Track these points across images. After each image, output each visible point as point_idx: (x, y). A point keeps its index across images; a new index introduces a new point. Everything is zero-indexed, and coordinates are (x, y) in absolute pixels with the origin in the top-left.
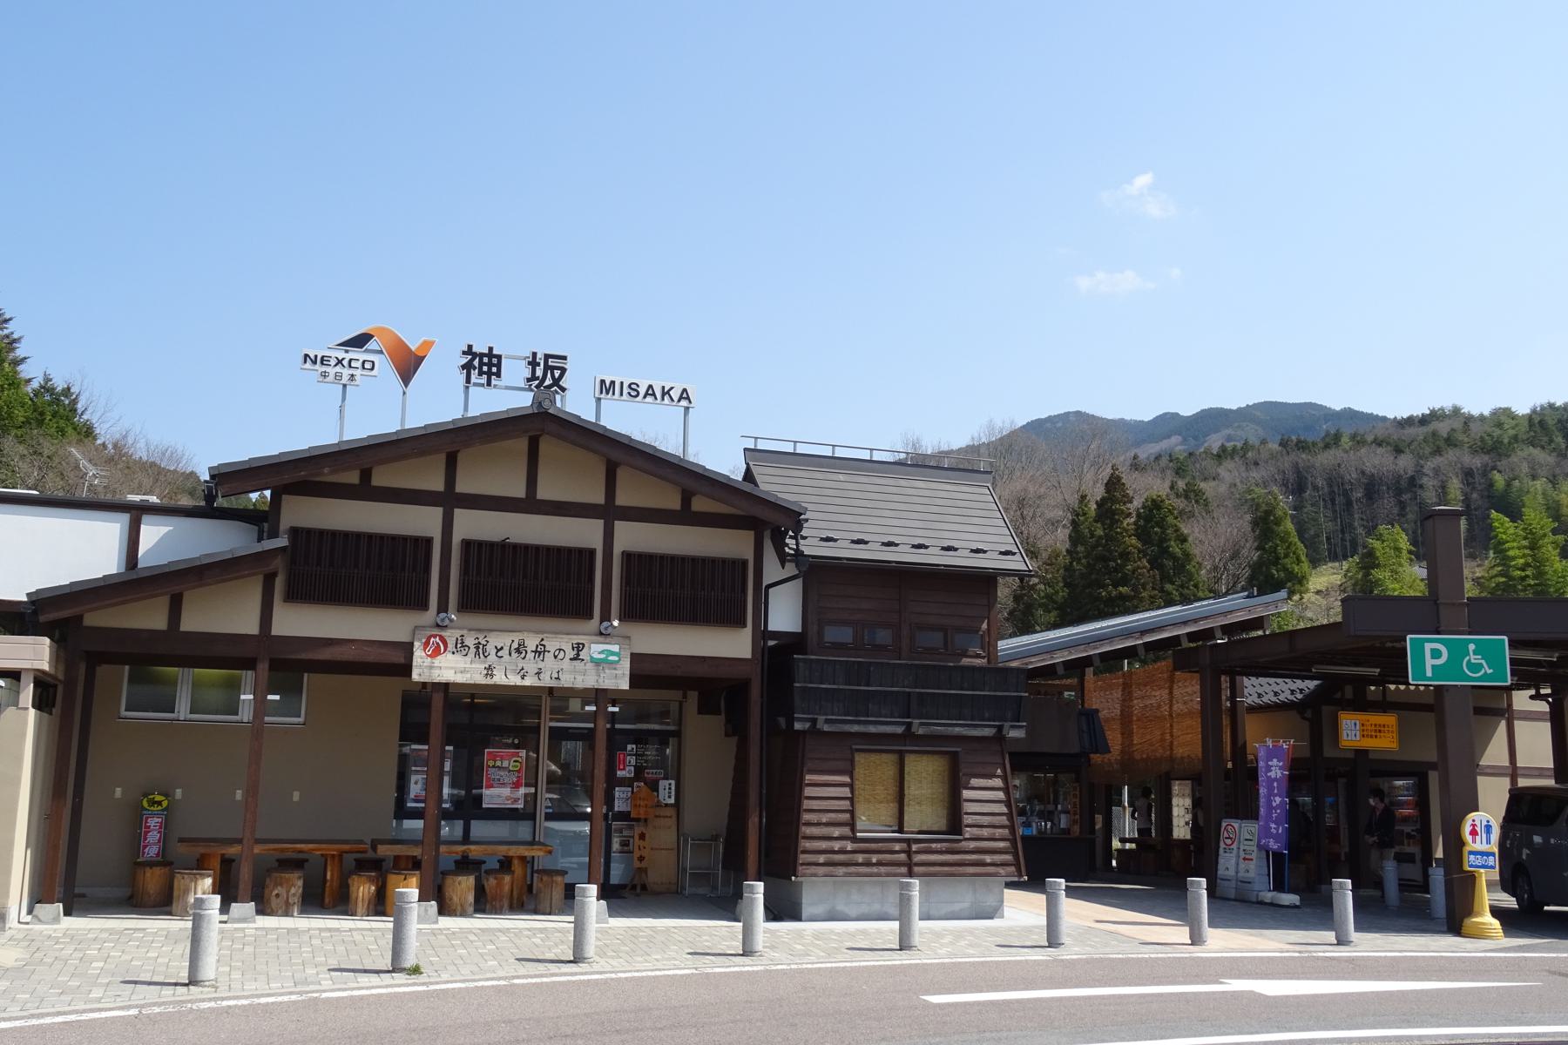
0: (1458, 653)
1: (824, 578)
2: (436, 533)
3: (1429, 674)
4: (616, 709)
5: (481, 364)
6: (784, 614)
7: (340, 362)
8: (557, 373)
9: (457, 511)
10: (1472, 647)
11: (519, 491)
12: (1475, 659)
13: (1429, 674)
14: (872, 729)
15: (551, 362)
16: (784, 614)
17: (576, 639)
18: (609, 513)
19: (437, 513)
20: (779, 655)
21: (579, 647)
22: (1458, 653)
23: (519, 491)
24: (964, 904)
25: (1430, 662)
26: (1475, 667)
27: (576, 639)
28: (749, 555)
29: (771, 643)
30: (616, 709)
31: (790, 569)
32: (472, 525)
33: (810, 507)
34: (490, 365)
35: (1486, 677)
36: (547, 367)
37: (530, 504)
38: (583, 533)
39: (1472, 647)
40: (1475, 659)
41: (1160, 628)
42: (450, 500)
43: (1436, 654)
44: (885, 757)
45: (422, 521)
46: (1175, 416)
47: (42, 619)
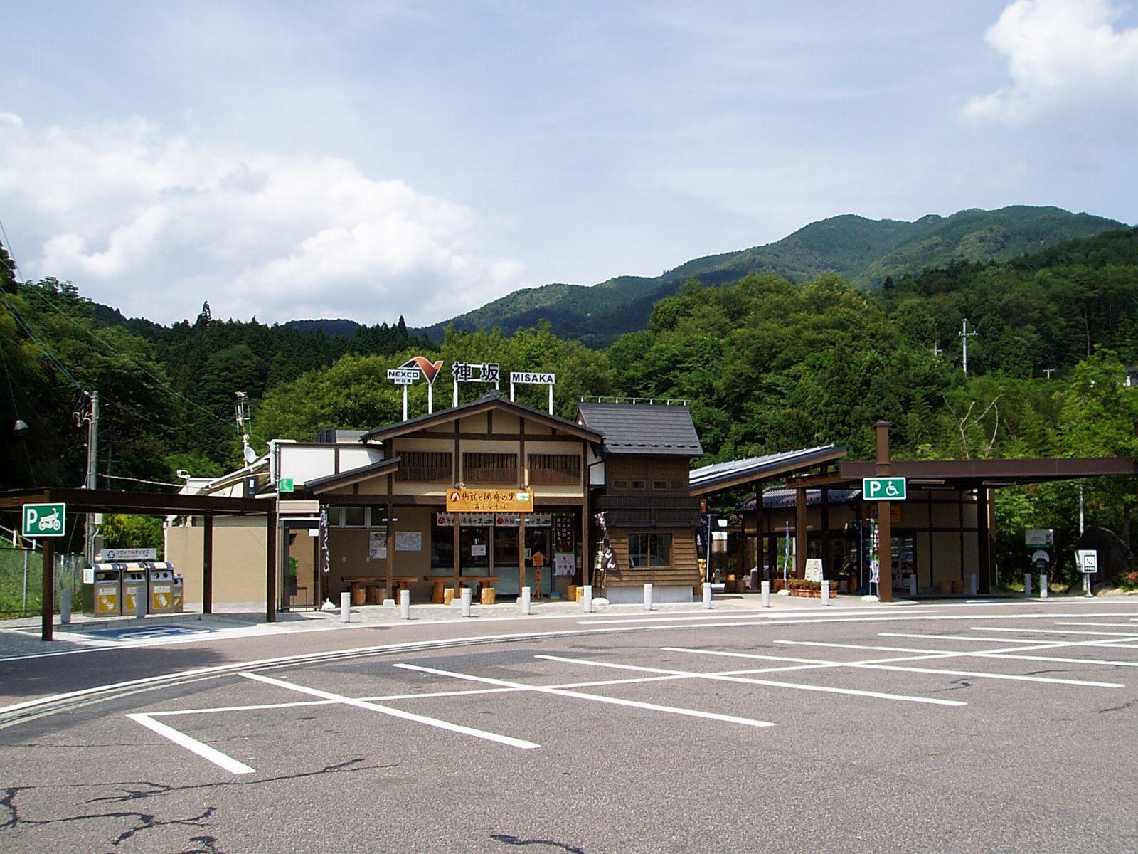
0: (884, 484)
1: (612, 461)
2: (453, 450)
3: (872, 494)
4: (384, 520)
5: (462, 371)
6: (597, 478)
7: (404, 374)
8: (494, 373)
9: (461, 441)
10: (890, 483)
11: (485, 431)
12: (892, 488)
13: (872, 494)
14: (1073, 624)
15: (491, 368)
16: (597, 478)
17: (511, 491)
18: (522, 438)
19: (453, 442)
20: (595, 494)
21: (512, 495)
22: (884, 484)
23: (485, 431)
24: (676, 598)
25: (873, 490)
26: (891, 492)
27: (511, 491)
28: (581, 454)
29: (592, 489)
30: (384, 520)
31: (599, 459)
32: (467, 446)
33: (607, 433)
34: (466, 371)
35: (895, 496)
36: (490, 370)
37: (490, 436)
38: (512, 447)
39: (890, 483)
40: (892, 488)
41: (118, 693)
42: (458, 436)
43: (875, 486)
44: (684, 589)
45: (447, 446)
46: (936, 218)
47: (315, 493)
